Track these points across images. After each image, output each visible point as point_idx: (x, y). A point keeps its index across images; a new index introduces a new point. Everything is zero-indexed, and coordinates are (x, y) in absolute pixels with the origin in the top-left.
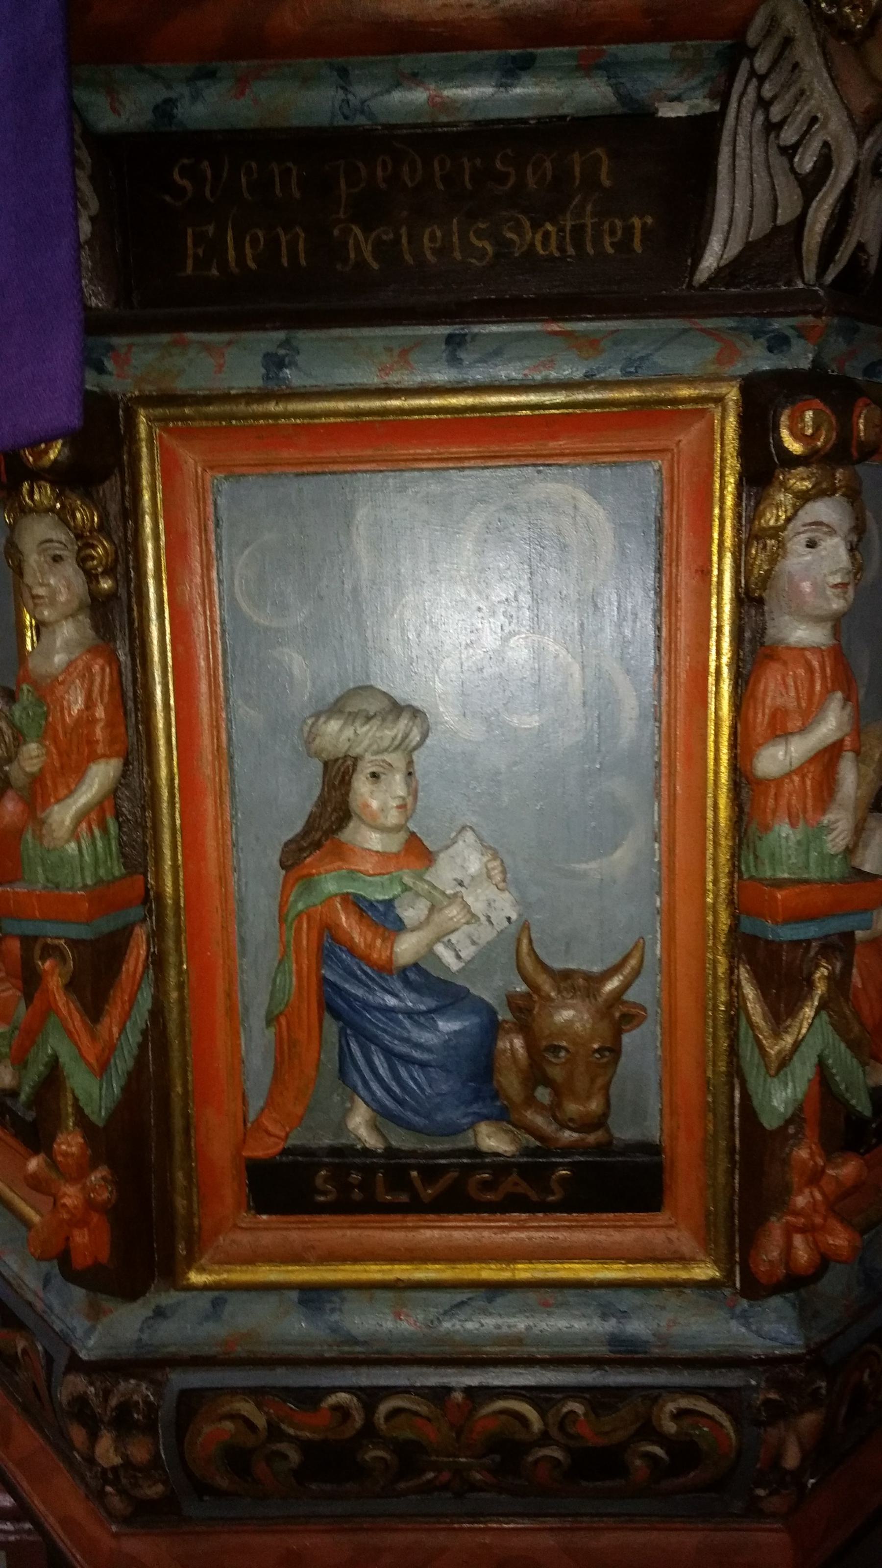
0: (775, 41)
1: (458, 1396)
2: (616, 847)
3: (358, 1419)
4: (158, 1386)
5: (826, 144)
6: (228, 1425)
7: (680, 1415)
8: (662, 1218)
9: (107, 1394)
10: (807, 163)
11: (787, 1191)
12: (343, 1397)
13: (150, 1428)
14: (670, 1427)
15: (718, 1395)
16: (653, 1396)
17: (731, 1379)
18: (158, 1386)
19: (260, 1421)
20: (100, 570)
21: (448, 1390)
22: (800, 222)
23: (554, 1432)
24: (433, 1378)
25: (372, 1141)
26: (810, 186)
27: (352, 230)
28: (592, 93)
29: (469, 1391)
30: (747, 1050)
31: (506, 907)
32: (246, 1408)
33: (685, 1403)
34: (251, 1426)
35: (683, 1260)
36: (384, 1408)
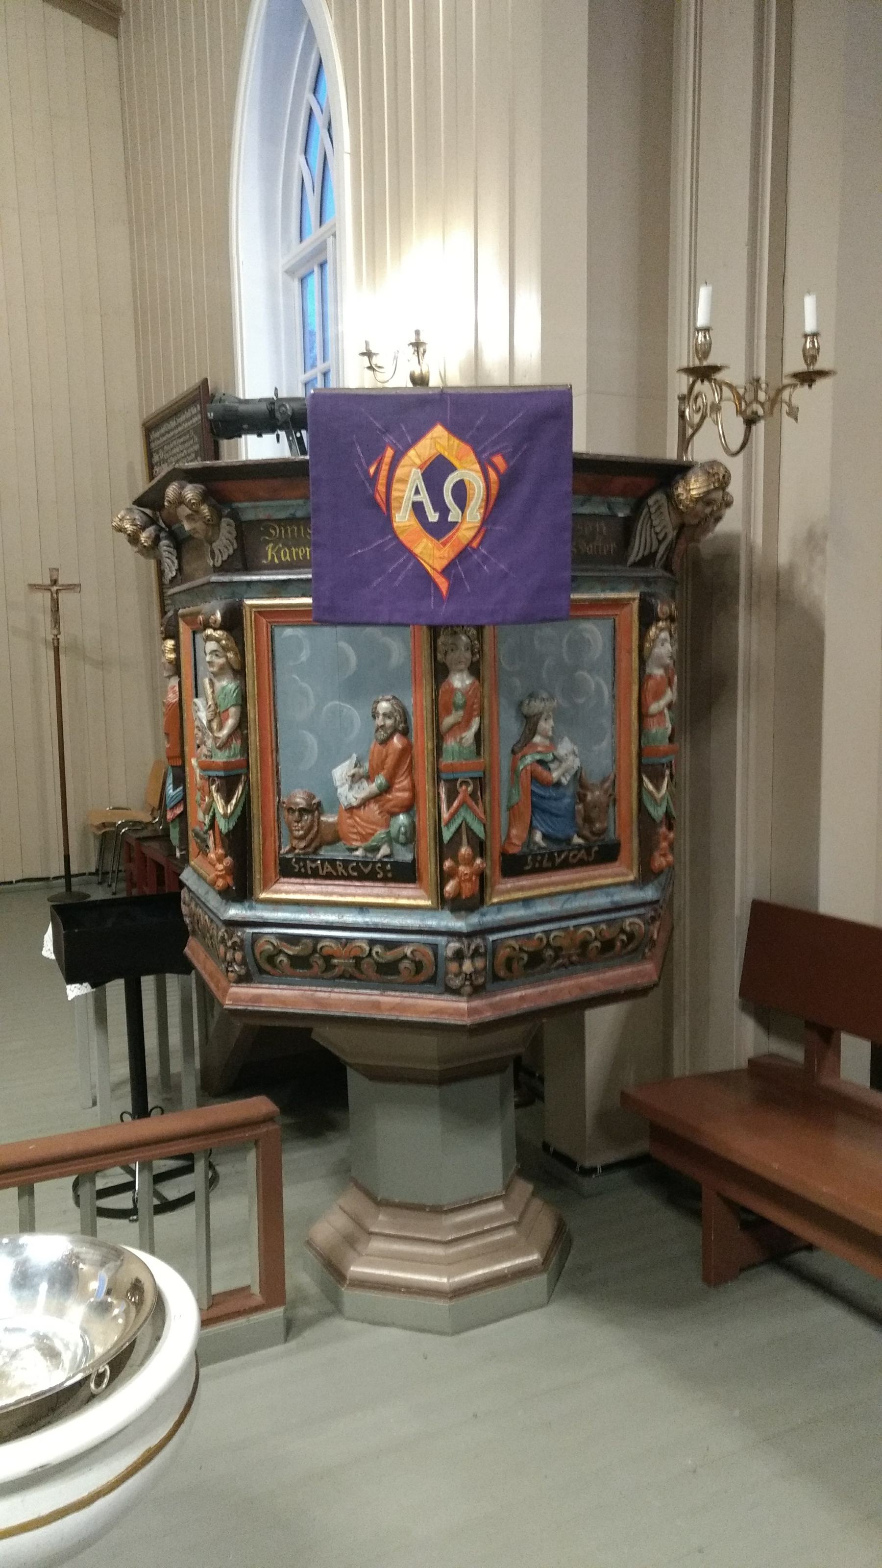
0: (656, 506)
1: (572, 929)
2: (602, 740)
3: (545, 941)
4: (484, 940)
5: (666, 534)
6: (508, 950)
7: (631, 924)
8: (617, 863)
9: (469, 945)
10: (661, 537)
11: (659, 842)
12: (540, 935)
13: (484, 955)
14: (628, 929)
15: (639, 916)
16: (623, 919)
17: (642, 911)
18: (484, 940)
19: (517, 947)
20: (660, 624)
21: (568, 927)
22: (656, 552)
23: (598, 936)
24: (564, 924)
25: (543, 844)
26: (660, 542)
27: (238, 508)
28: (603, 510)
29: (575, 926)
30: (645, 797)
31: (577, 763)
32: (513, 943)
33: (631, 920)
34: (514, 949)
35: (627, 875)
36: (552, 936)
